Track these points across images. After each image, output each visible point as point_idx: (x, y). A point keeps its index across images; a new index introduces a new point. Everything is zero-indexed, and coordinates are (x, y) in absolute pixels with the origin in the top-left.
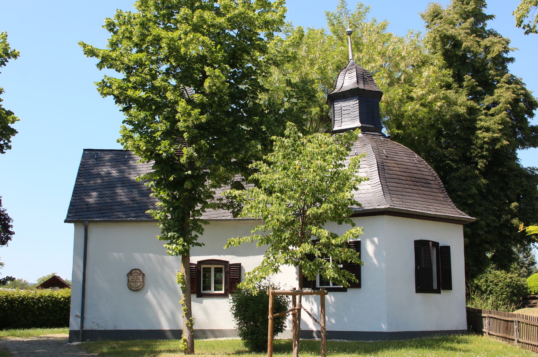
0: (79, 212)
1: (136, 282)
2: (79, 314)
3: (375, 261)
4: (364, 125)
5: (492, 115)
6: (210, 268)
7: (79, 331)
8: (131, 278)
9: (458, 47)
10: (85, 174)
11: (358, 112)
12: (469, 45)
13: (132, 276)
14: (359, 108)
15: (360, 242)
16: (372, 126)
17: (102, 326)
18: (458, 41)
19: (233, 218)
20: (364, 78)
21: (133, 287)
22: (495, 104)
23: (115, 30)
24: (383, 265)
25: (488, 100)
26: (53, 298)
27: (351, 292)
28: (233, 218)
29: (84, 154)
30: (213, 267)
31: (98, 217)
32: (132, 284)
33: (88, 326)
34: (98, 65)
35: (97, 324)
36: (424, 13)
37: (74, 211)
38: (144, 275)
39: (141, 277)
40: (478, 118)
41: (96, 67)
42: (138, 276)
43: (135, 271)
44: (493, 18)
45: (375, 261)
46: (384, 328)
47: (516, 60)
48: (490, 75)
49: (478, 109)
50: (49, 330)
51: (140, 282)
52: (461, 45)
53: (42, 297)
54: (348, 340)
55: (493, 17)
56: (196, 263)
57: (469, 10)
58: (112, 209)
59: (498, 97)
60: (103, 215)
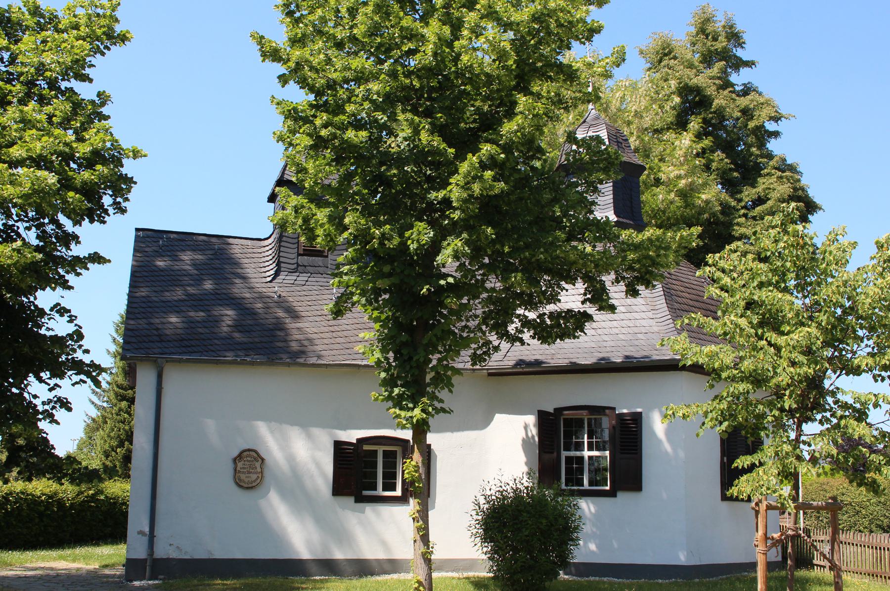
0: (145, 342)
1: (249, 473)
2: (147, 529)
3: (667, 447)
4: (621, 220)
5: (754, 218)
6: (376, 451)
7: (145, 560)
8: (240, 465)
9: (705, 106)
10: (145, 274)
11: (612, 196)
12: (723, 105)
13: (242, 462)
14: (613, 190)
15: (640, 413)
16: (631, 222)
17: (186, 553)
18: (705, 96)
19: (471, 367)
20: (618, 142)
21: (244, 482)
22: (760, 201)
23: (297, 15)
24: (681, 454)
25: (748, 194)
26: (28, 495)
27: (623, 497)
28: (471, 367)
29: (137, 237)
30: (381, 449)
31: (180, 354)
32: (243, 476)
33: (163, 551)
34: (279, 77)
35: (178, 547)
36: (644, 48)
37: (133, 340)
38: (263, 460)
39: (258, 464)
40: (735, 221)
41: (277, 80)
42: (253, 461)
43: (248, 453)
44: (753, 66)
45: (667, 447)
46: (682, 558)
47: (782, 136)
48: (752, 154)
49: (734, 208)
50: (54, 553)
51: (256, 473)
52: (711, 104)
53: (11, 493)
54: (628, 578)
55: (754, 64)
56: (355, 441)
57: (717, 49)
58: (204, 340)
59: (764, 190)
60: (190, 349)
